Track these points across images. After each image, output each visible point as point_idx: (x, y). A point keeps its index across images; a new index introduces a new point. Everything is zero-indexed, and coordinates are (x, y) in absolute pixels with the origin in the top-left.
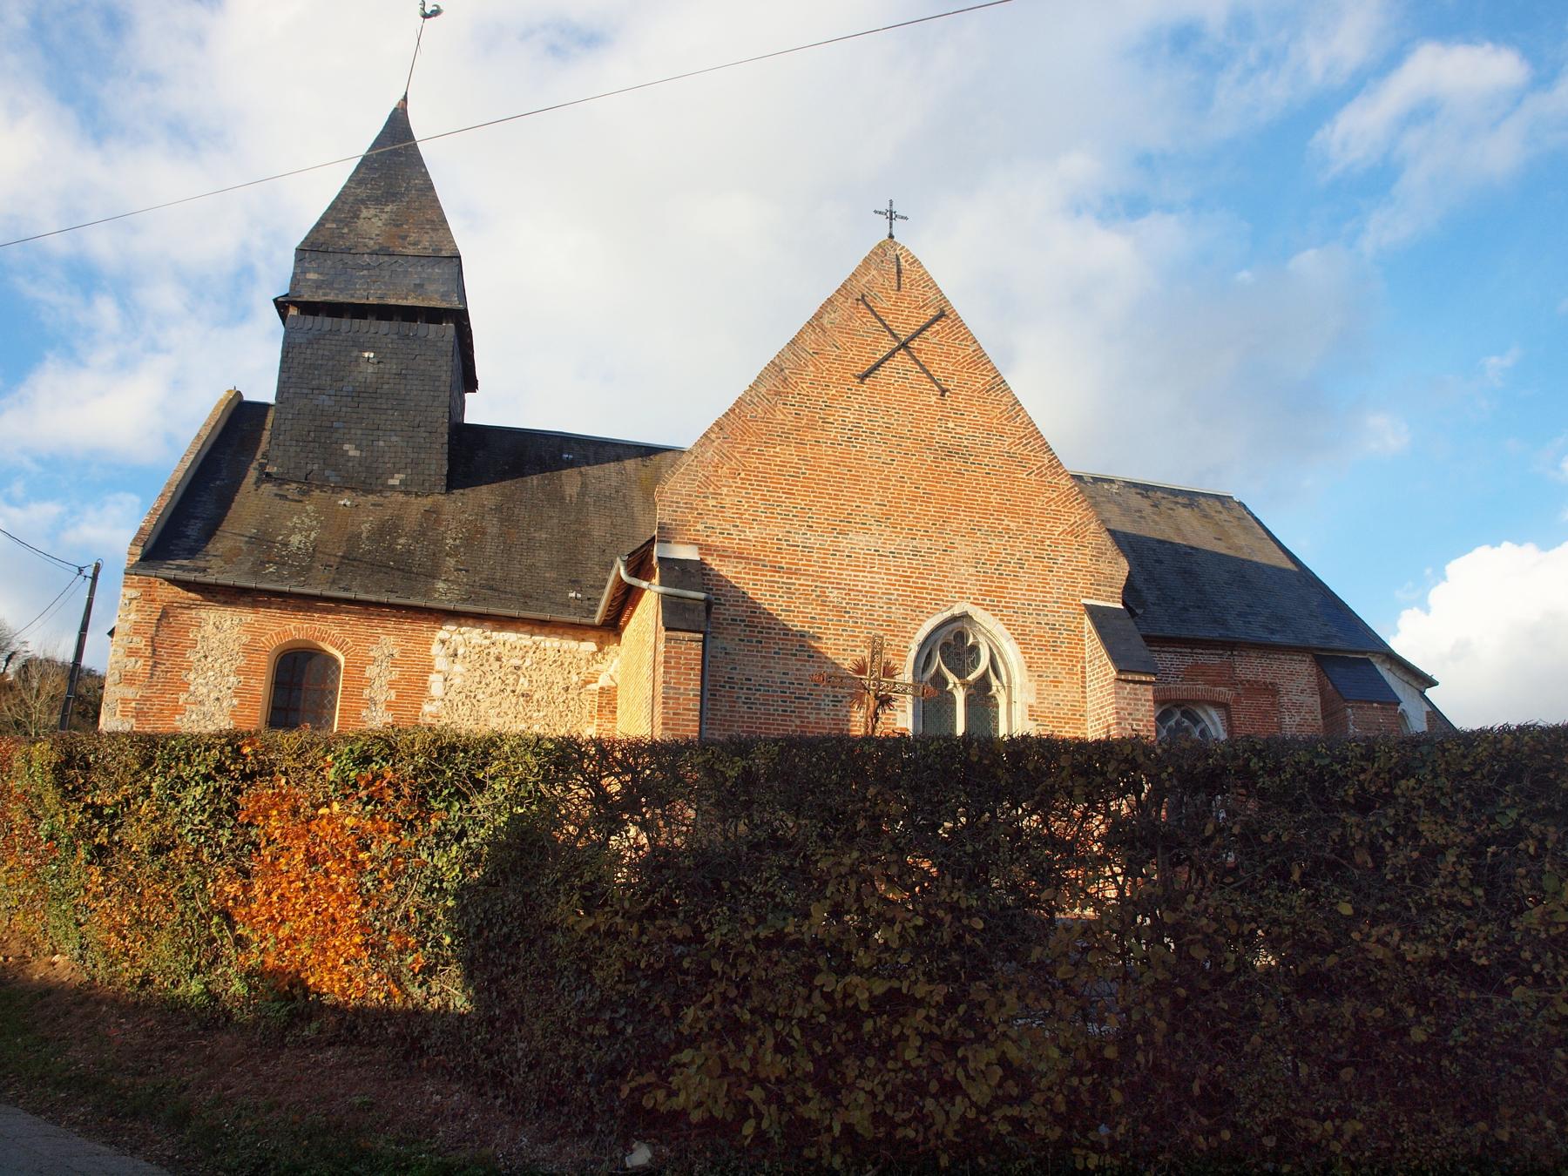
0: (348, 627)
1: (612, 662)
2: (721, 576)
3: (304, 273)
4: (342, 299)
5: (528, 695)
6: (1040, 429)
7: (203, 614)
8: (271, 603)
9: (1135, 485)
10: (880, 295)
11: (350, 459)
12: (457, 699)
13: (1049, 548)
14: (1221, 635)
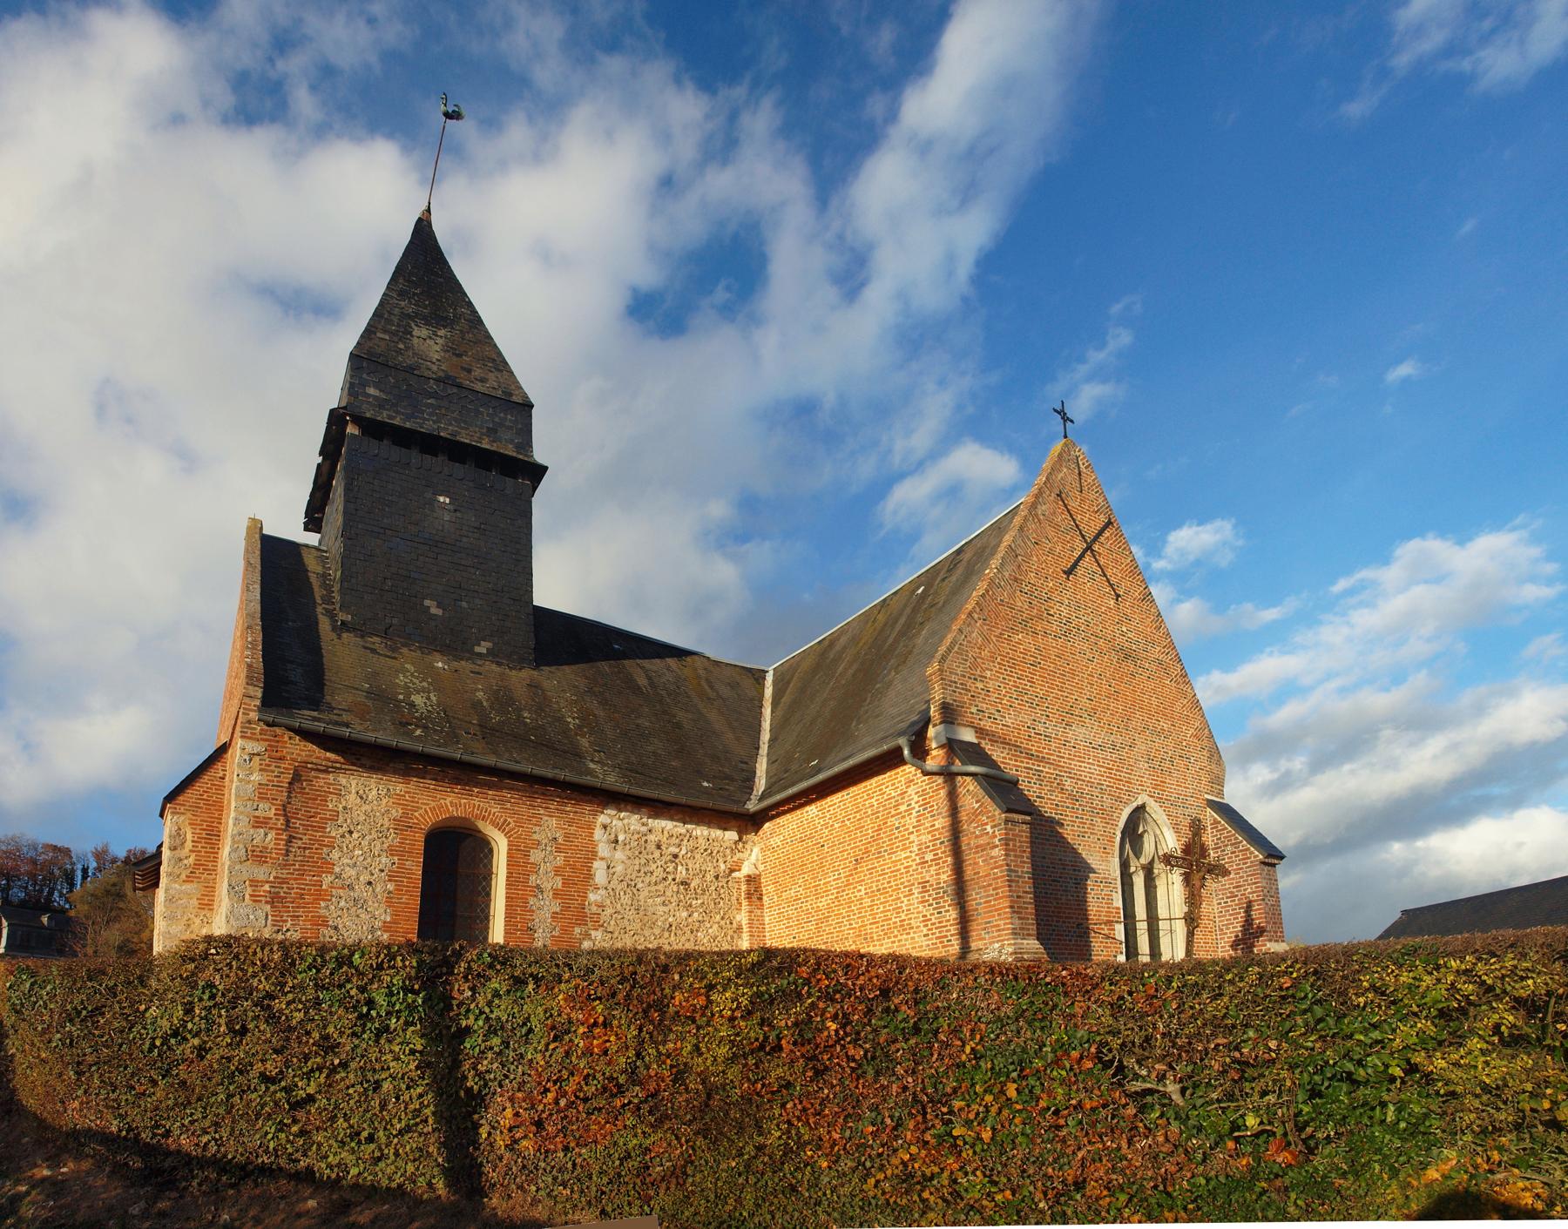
5: (686, 884)
8: (426, 772)
11: (433, 617)
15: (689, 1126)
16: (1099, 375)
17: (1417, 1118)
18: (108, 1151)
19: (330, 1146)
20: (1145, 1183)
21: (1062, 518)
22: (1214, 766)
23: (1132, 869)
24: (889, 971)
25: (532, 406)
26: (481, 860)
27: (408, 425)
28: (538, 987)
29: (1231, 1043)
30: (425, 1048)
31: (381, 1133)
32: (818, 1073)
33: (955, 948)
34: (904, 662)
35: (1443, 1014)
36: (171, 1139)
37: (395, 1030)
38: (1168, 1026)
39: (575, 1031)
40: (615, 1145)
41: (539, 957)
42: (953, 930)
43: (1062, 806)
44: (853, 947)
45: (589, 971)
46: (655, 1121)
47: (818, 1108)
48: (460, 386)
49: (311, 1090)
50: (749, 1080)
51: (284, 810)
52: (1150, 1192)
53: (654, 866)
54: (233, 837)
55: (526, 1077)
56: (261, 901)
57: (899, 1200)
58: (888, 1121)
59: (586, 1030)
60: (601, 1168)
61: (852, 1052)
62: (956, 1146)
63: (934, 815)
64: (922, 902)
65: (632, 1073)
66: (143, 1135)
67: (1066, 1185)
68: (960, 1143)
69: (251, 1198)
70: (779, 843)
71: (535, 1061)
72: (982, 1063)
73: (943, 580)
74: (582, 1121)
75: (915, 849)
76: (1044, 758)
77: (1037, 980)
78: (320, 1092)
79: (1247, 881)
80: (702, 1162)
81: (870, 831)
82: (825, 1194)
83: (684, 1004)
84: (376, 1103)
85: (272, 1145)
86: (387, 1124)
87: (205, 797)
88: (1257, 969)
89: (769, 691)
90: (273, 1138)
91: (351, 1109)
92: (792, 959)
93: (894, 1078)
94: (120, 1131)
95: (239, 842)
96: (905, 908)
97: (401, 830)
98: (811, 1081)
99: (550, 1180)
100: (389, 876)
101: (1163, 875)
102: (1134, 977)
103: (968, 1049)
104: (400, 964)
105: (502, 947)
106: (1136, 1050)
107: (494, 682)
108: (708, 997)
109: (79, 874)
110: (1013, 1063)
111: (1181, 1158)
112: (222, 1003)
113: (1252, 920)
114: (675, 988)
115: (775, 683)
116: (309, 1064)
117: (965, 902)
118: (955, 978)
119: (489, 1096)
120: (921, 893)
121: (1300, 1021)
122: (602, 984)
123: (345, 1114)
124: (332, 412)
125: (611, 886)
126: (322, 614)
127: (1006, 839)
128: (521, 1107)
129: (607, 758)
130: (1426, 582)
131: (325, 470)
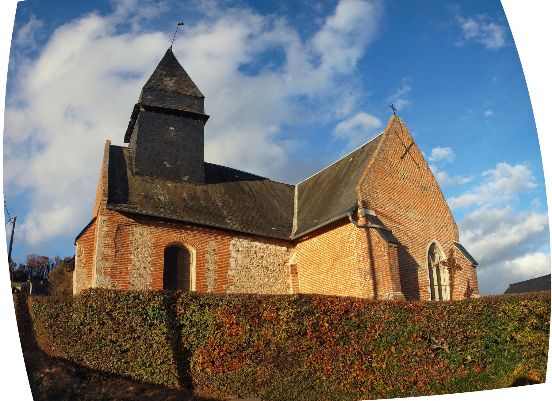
0: (196, 237)
1: (292, 255)
5: (267, 268)
8: (165, 225)
11: (168, 168)
12: (240, 269)
15: (272, 364)
16: (402, 97)
17: (513, 354)
18: (65, 365)
19: (136, 368)
20: (436, 381)
21: (397, 140)
22: (455, 230)
23: (432, 266)
24: (348, 303)
25: (204, 98)
26: (186, 258)
27: (161, 106)
28: (210, 308)
29: (464, 330)
30: (168, 332)
31: (154, 364)
32: (322, 343)
33: (372, 295)
34: (347, 185)
35: (520, 320)
36: (83, 362)
37: (156, 324)
38: (445, 324)
39: (225, 326)
40: (243, 371)
41: (210, 297)
42: (372, 287)
43: (408, 242)
44: (334, 294)
45: (230, 302)
46: (258, 362)
47: (322, 357)
48: (179, 93)
49: (128, 346)
50: (295, 346)
51: (115, 241)
52: (438, 384)
53: (254, 261)
54: (98, 251)
55: (207, 344)
56: (107, 275)
57: (352, 391)
58: (348, 362)
59: (229, 326)
60: (238, 379)
61: (334, 335)
62: (373, 370)
63: (362, 243)
64: (359, 276)
65: (248, 343)
66: (75, 360)
67: (411, 383)
68: (375, 369)
69: (111, 385)
70: (303, 252)
71: (210, 338)
72: (383, 339)
73: (359, 157)
74: (229, 361)
75: (356, 255)
76: (400, 223)
77: (402, 307)
78: (131, 347)
79: (467, 272)
80: (277, 377)
81: (338, 248)
82: (325, 389)
83: (268, 316)
84: (151, 352)
85: (116, 366)
86: (155, 360)
87: (88, 237)
88: (471, 304)
89: (296, 193)
90: (116, 364)
91: (142, 354)
92: (310, 298)
93: (350, 345)
94: (68, 358)
95: (99, 253)
96: (353, 279)
97: (156, 247)
98: (319, 347)
99: (218, 383)
100: (152, 265)
101: (442, 269)
102: (434, 306)
103: (377, 334)
104: (157, 299)
105: (195, 293)
106: (435, 333)
107: (190, 190)
108: (277, 313)
109: (51, 266)
110: (393, 339)
111: (448, 372)
112: (96, 313)
113: (470, 286)
114: (264, 309)
115: (298, 190)
116: (126, 336)
117: (375, 277)
118: (373, 306)
119: (193, 351)
120: (359, 273)
121: (483, 323)
122: (235, 308)
123: (140, 356)
124: (136, 105)
125: (237, 268)
126: (129, 170)
127: (389, 253)
128: (205, 355)
129: (234, 218)
130: (506, 177)
131: (132, 123)
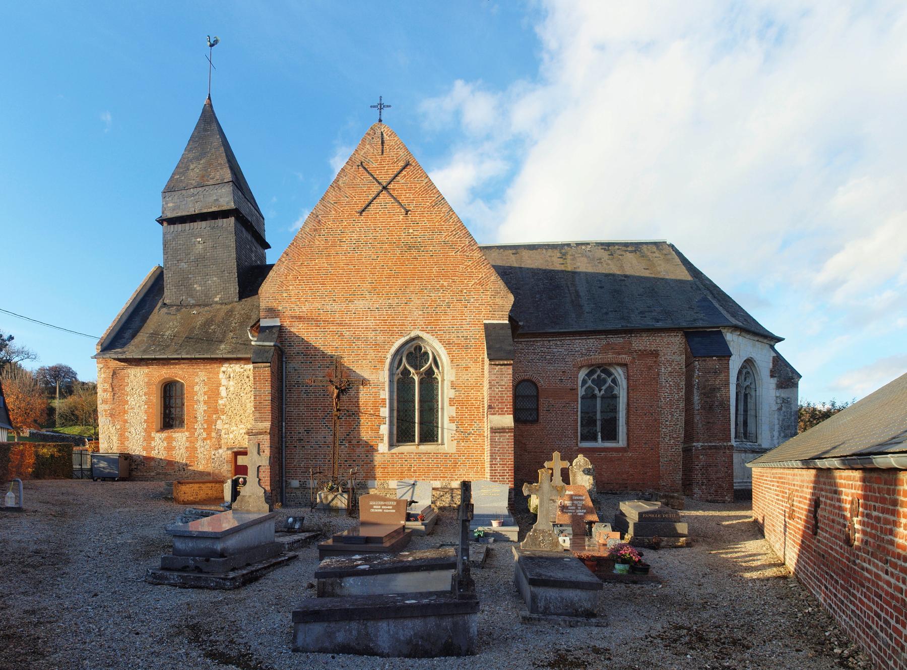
0: (185, 370)
2: (291, 332)
3: (167, 204)
4: (184, 213)
6: (464, 224)
7: (129, 371)
9: (602, 244)
10: (371, 160)
13: (465, 294)
14: (622, 326)
